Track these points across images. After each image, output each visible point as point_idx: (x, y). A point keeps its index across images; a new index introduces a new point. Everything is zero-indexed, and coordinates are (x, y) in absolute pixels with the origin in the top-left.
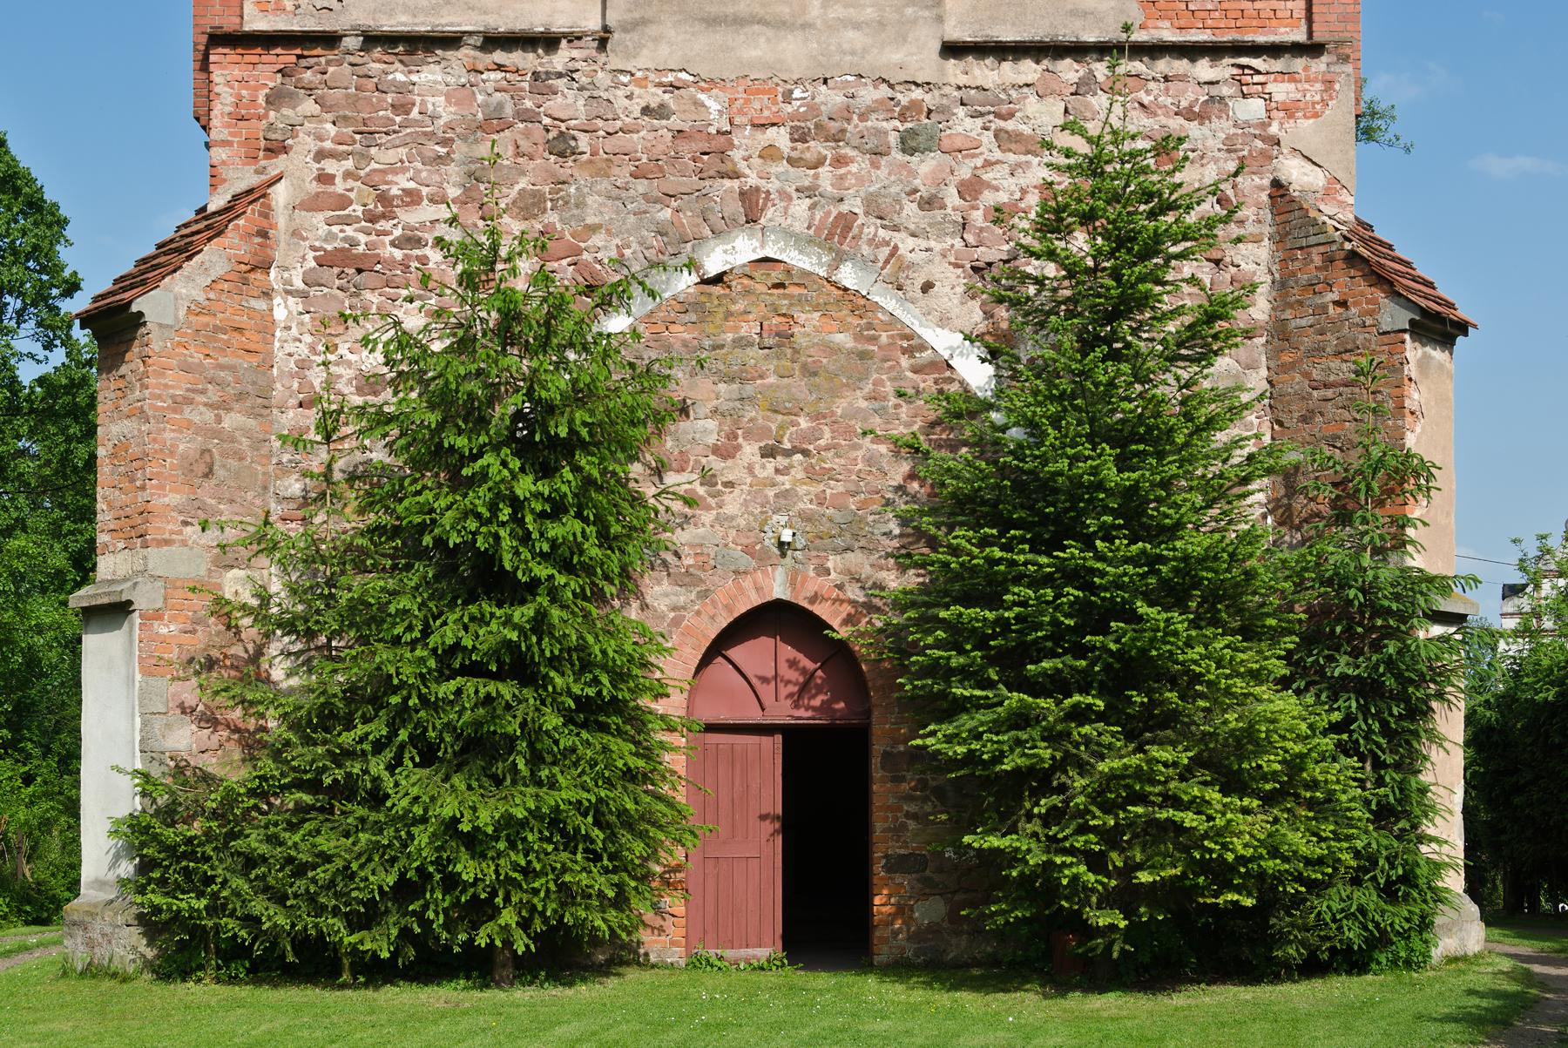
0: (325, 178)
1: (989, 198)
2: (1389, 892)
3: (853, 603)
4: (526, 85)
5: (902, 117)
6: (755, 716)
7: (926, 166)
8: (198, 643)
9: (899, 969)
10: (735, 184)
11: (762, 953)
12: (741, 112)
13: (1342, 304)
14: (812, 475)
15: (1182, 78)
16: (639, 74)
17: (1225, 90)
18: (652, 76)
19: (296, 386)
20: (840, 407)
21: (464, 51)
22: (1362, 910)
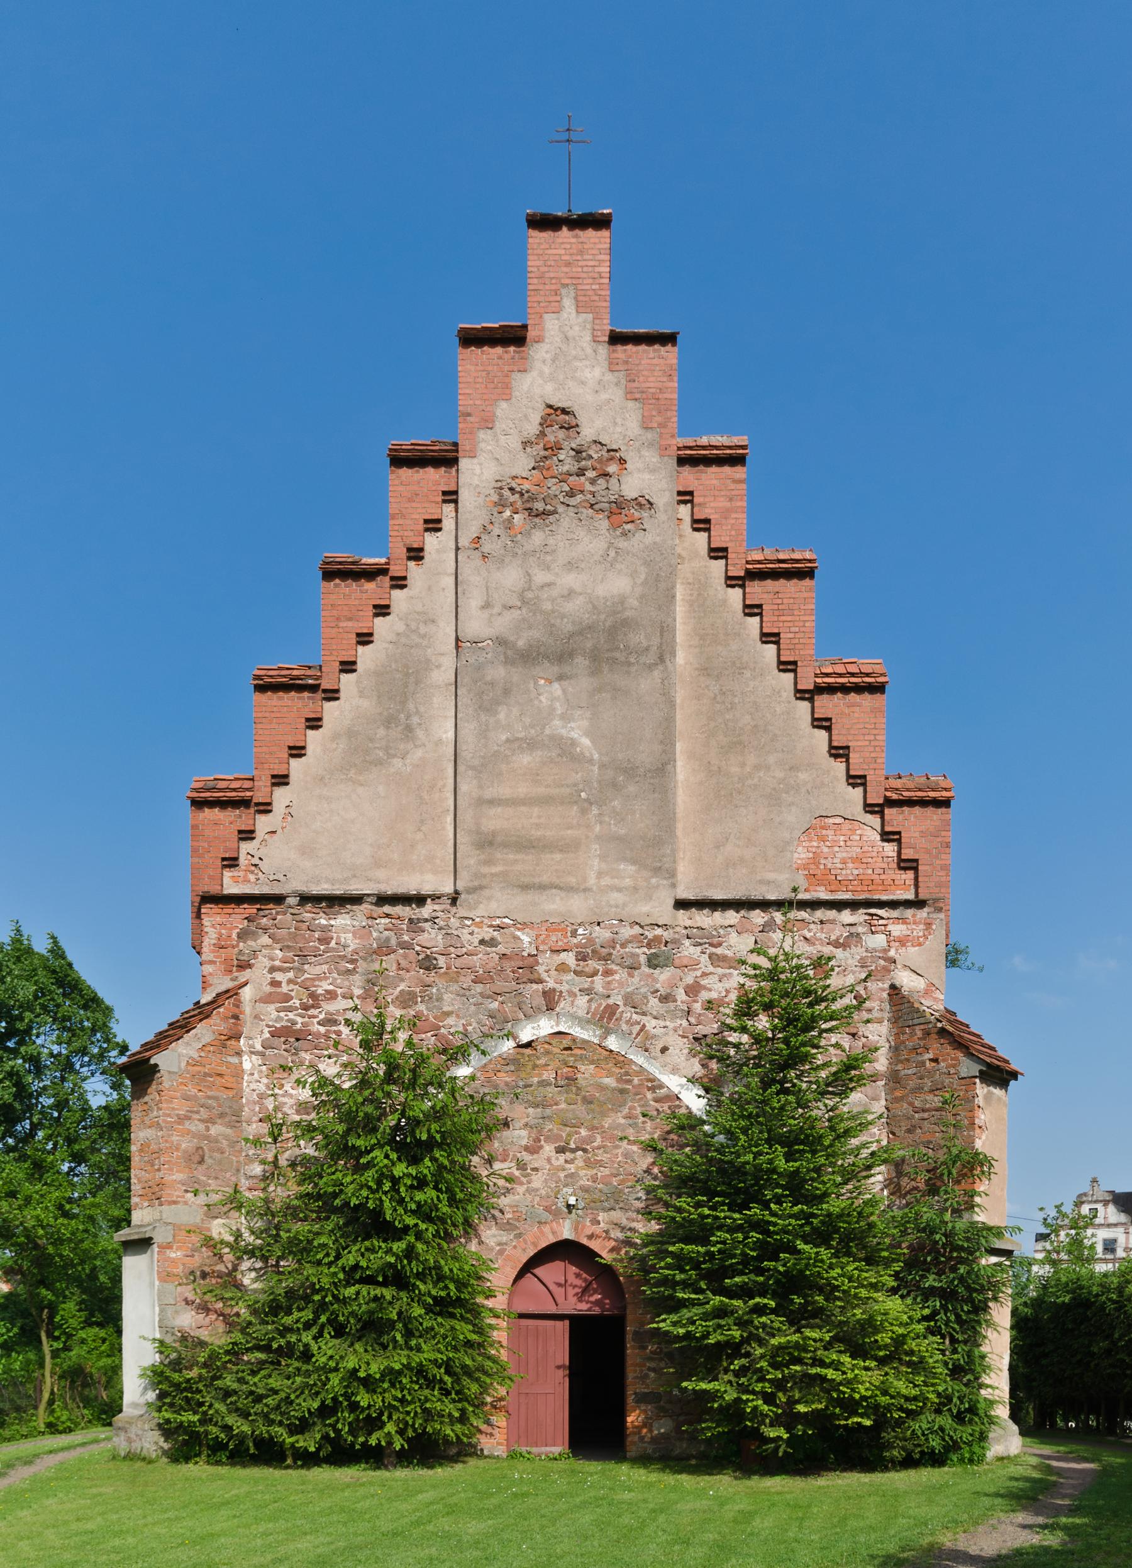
0: (275, 984)
1: (705, 995)
2: (959, 1418)
4: (405, 927)
5: (649, 946)
6: (552, 1309)
7: (663, 976)
9: (643, 1460)
10: (540, 987)
11: (556, 1450)
12: (543, 942)
13: (935, 1060)
14: (589, 1164)
15: (832, 922)
16: (478, 920)
17: (860, 929)
18: (486, 921)
19: (257, 1109)
20: (607, 1123)
22: (942, 1429)
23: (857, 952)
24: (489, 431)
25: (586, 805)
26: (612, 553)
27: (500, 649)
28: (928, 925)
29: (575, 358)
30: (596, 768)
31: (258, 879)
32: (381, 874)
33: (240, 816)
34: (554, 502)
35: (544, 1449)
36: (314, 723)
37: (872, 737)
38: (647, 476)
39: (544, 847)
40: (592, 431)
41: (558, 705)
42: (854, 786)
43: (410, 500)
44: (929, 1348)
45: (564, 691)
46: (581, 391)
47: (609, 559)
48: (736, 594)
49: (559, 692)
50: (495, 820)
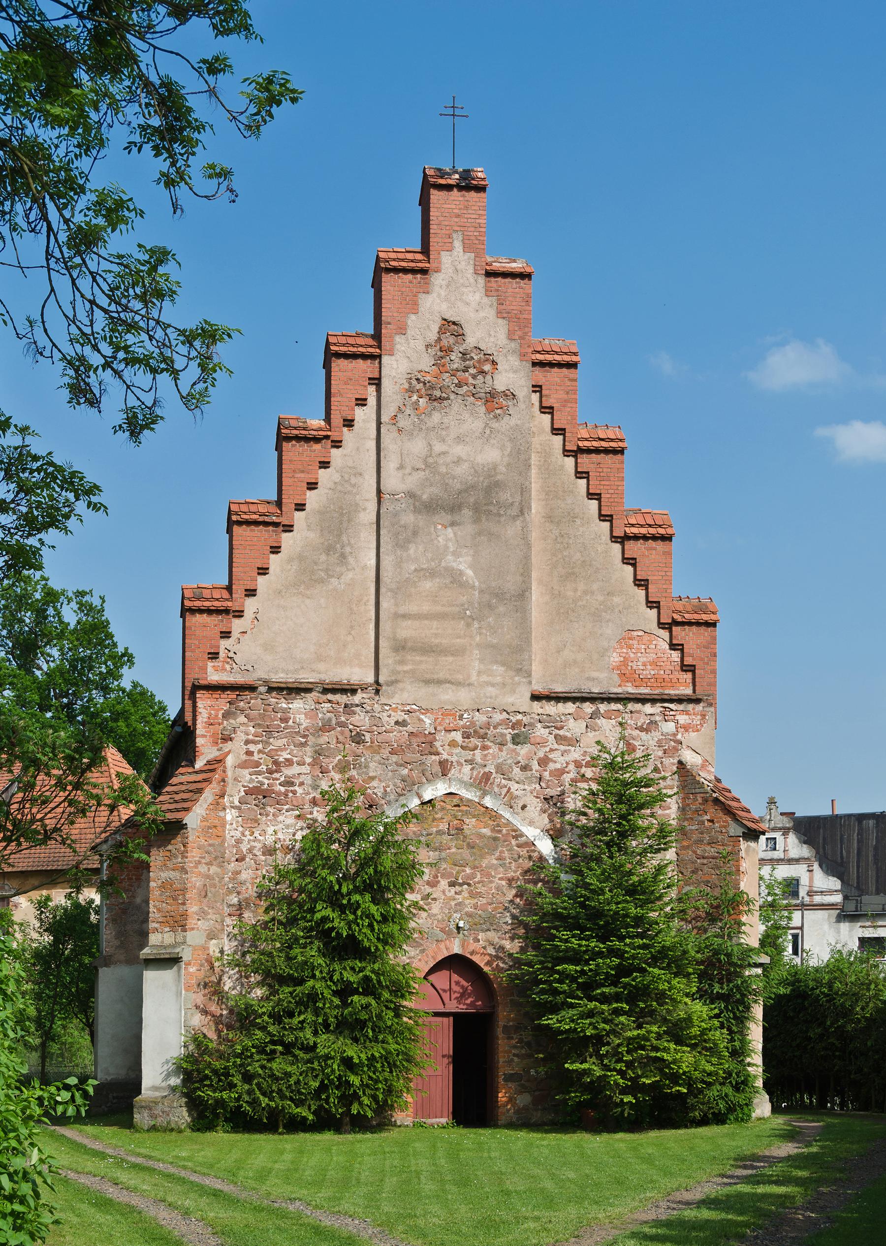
0: (249, 753)
1: (552, 766)
2: (737, 1088)
3: (490, 955)
4: (341, 710)
5: (513, 728)
6: (441, 1009)
7: (523, 750)
8: (201, 974)
9: (511, 1125)
10: (437, 758)
11: (444, 1121)
12: (440, 724)
13: (711, 821)
14: (472, 895)
15: (639, 712)
16: (394, 706)
17: (658, 718)
18: (400, 707)
19: (235, 851)
20: (484, 863)
21: (314, 693)
22: (726, 1095)
23: (656, 735)
24: (403, 336)
25: (470, 620)
26: (488, 432)
27: (411, 501)
28: (703, 716)
29: (463, 285)
30: (477, 593)
31: (232, 669)
32: (321, 666)
33: (222, 621)
34: (447, 391)
35: (434, 1120)
36: (276, 550)
37: (664, 574)
38: (511, 375)
39: (441, 651)
40: (474, 339)
41: (450, 544)
42: (651, 608)
43: (346, 383)
44: (719, 1036)
45: (455, 533)
46: (466, 310)
47: (486, 435)
48: (570, 461)
49: (451, 535)
50: (407, 630)
